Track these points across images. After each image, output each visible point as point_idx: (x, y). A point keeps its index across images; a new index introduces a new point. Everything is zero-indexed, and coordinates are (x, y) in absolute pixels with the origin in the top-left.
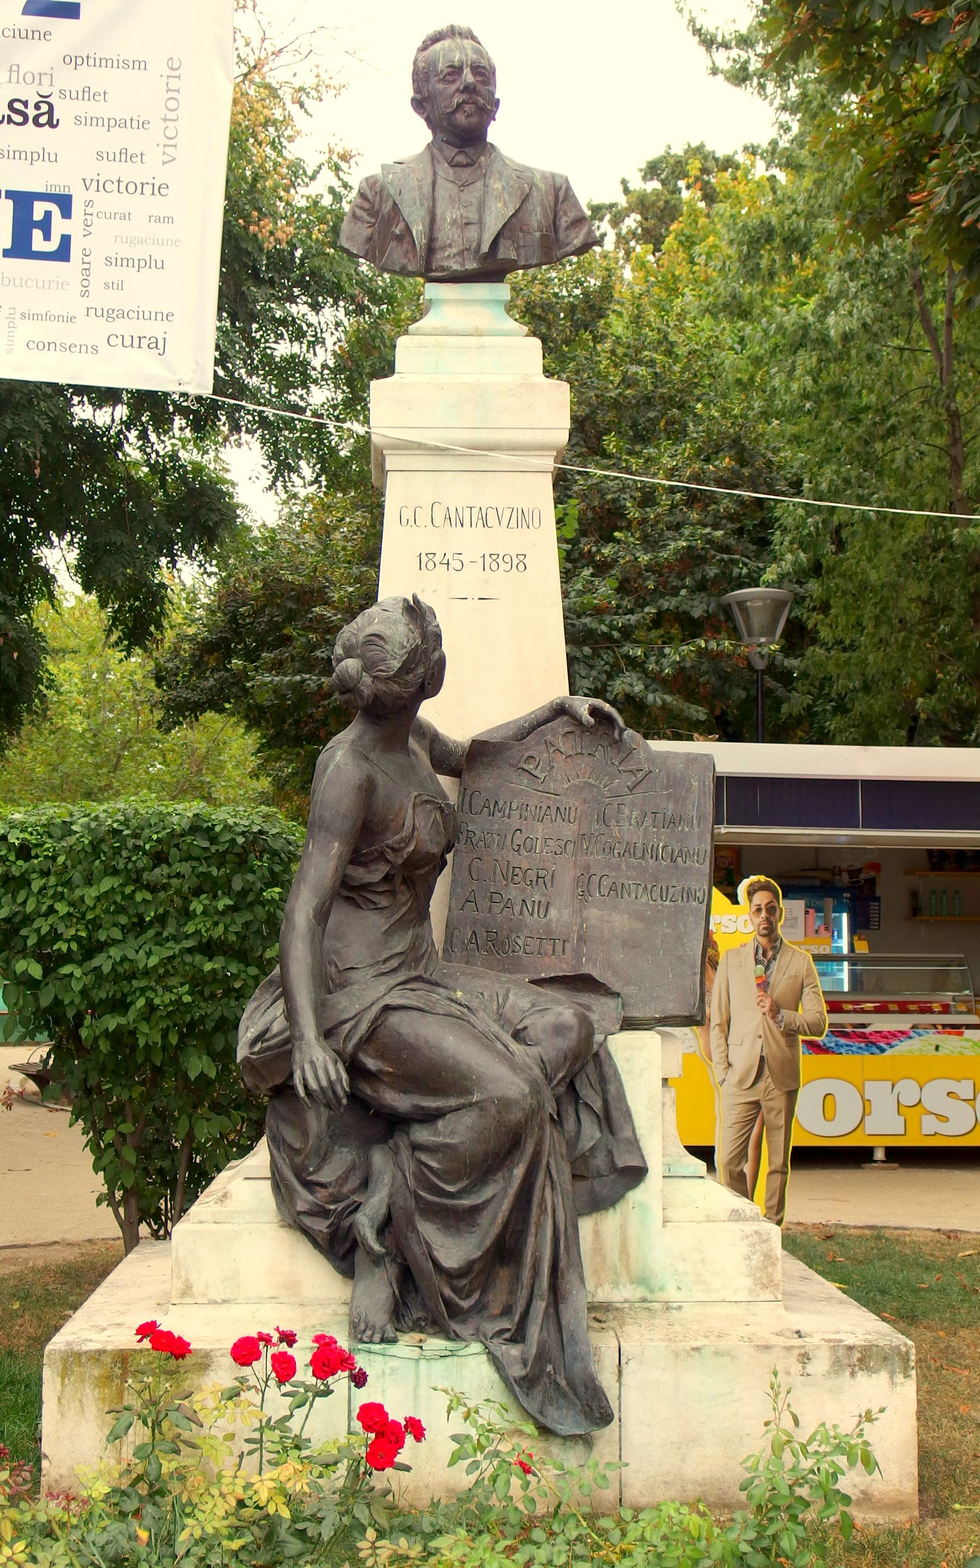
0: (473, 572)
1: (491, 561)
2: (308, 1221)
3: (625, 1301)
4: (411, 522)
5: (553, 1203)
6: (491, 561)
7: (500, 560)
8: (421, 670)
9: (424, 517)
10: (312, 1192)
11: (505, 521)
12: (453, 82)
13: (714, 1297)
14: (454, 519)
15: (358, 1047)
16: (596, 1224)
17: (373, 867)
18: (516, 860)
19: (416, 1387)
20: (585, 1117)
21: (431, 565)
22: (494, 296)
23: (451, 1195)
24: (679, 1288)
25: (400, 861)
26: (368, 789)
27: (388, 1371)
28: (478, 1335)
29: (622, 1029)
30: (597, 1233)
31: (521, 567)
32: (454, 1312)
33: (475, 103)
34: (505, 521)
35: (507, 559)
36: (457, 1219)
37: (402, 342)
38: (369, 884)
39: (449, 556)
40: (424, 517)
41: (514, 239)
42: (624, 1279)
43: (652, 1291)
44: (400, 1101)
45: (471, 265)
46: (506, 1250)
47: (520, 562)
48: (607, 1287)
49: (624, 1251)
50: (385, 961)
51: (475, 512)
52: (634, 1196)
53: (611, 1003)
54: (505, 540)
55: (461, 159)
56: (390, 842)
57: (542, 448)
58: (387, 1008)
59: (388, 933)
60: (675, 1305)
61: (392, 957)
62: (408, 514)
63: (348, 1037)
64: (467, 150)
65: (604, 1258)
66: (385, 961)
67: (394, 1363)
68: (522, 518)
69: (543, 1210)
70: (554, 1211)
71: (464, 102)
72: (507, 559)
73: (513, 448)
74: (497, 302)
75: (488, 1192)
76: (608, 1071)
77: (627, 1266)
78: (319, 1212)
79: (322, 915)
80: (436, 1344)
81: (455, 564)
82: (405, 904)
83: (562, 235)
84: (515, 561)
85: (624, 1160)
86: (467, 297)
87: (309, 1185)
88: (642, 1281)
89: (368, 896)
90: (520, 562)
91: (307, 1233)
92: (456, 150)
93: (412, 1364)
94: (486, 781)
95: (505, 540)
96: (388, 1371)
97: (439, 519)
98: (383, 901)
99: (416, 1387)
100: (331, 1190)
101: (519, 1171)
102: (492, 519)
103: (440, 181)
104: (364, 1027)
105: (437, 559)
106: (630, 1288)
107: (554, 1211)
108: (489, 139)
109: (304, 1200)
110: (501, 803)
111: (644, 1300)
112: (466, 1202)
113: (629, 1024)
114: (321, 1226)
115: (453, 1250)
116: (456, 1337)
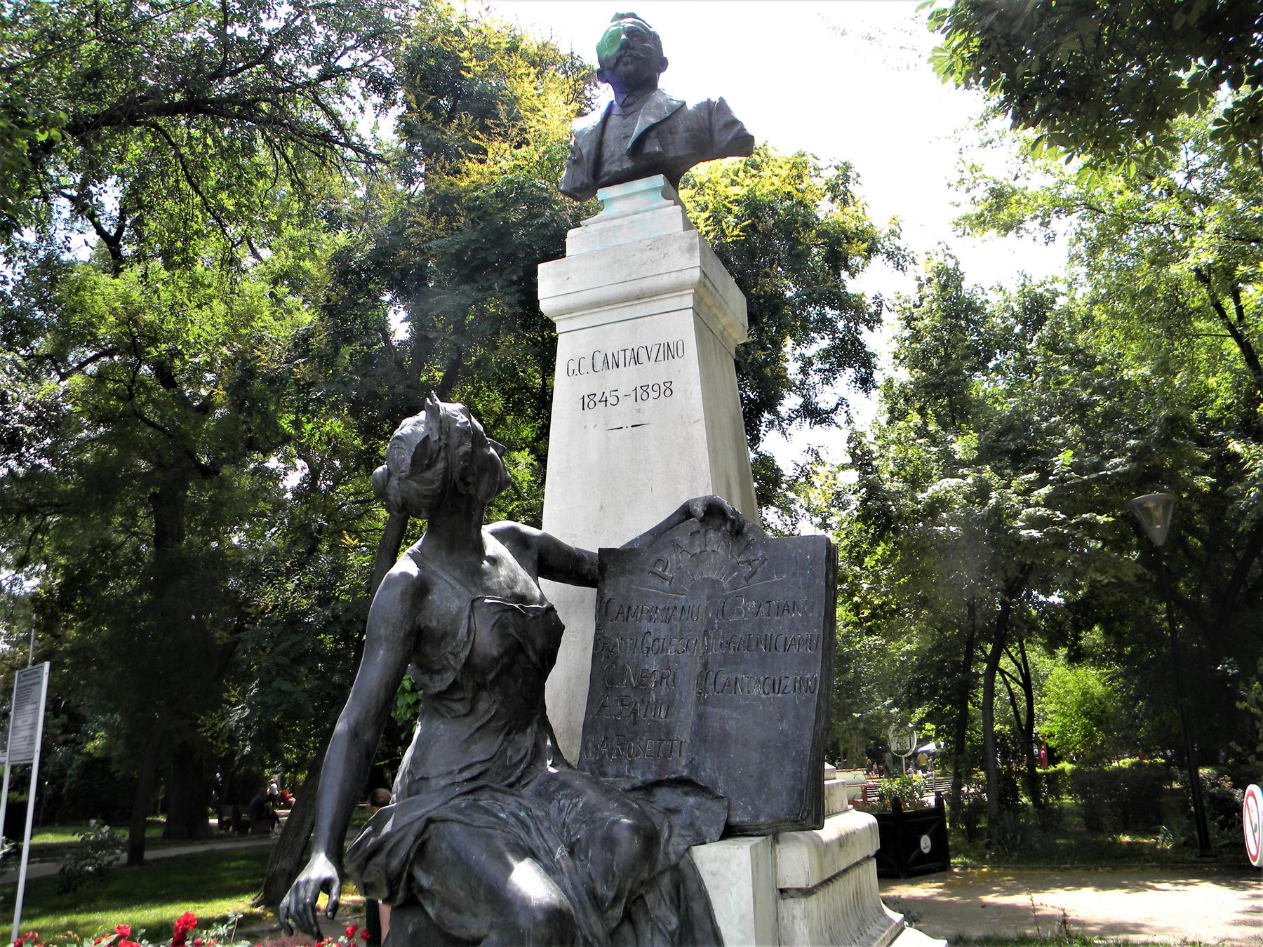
0: (627, 405)
1: (641, 393)
4: (576, 371)
6: (641, 393)
7: (650, 390)
8: (440, 465)
11: (653, 356)
14: (611, 363)
22: (651, 186)
25: (459, 667)
31: (668, 392)
34: (653, 356)
35: (656, 388)
37: (571, 233)
38: (441, 693)
41: (660, 137)
45: (628, 164)
50: (461, 771)
51: (628, 353)
53: (717, 807)
54: (652, 372)
58: (430, 821)
59: (470, 740)
68: (670, 351)
72: (656, 388)
74: (655, 189)
81: (612, 400)
83: (716, 136)
94: (618, 587)
95: (652, 372)
98: (460, 708)
102: (643, 357)
104: (410, 839)
105: (597, 399)
108: (659, 86)
110: (634, 608)
113: (730, 832)
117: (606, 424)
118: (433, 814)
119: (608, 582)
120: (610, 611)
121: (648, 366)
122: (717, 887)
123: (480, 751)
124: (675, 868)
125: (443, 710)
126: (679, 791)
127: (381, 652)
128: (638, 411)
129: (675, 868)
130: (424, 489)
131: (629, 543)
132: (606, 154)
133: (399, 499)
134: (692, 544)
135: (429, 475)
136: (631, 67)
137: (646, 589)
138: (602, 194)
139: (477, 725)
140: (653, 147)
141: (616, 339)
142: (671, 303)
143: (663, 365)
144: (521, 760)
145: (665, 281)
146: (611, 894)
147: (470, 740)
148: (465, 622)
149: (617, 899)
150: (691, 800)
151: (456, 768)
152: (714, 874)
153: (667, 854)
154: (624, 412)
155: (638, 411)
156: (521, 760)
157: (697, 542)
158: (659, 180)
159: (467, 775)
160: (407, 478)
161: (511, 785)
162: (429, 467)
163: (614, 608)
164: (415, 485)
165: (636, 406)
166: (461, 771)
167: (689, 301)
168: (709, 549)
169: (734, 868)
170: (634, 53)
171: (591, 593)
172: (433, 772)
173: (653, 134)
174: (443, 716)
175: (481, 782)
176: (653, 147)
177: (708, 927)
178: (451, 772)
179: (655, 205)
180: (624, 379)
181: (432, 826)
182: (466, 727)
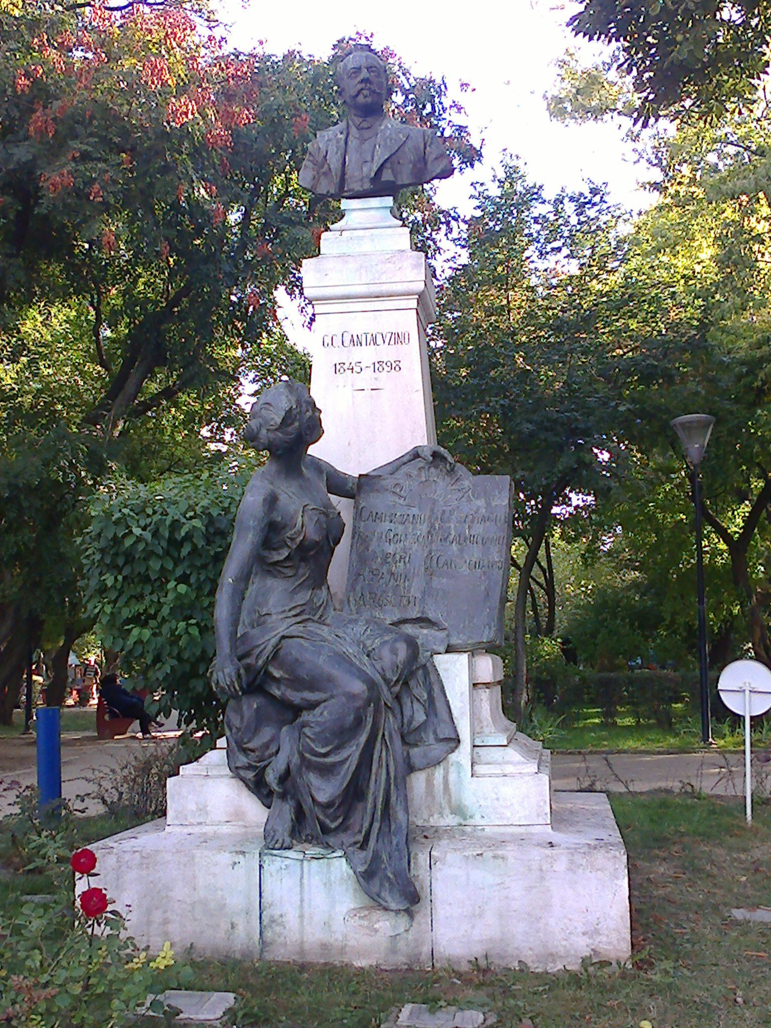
0: (368, 373)
2: (242, 773)
5: (387, 760)
6: (378, 366)
8: (297, 424)
9: (337, 341)
10: (247, 756)
11: (387, 341)
12: (356, 77)
13: (505, 822)
14: (356, 341)
15: (267, 663)
17: (281, 551)
18: (390, 549)
19: (302, 878)
20: (416, 705)
21: (342, 370)
22: (383, 205)
23: (325, 755)
24: (483, 817)
25: (294, 547)
26: (272, 501)
27: (284, 867)
28: (341, 846)
29: (447, 652)
30: (429, 782)
31: (397, 368)
32: (325, 830)
34: (387, 341)
35: (389, 364)
36: (326, 771)
38: (278, 561)
39: (353, 364)
40: (337, 341)
42: (447, 811)
43: (465, 819)
44: (295, 697)
45: (367, 186)
46: (355, 792)
47: (395, 366)
48: (436, 816)
50: (290, 610)
51: (369, 337)
54: (387, 352)
55: (365, 125)
56: (288, 535)
57: (407, 294)
58: (283, 637)
61: (295, 607)
62: (328, 340)
63: (257, 658)
64: (367, 119)
65: (434, 798)
67: (288, 862)
68: (398, 338)
69: (380, 766)
70: (387, 765)
71: (362, 89)
72: (389, 364)
73: (390, 295)
75: (344, 754)
77: (449, 801)
78: (249, 767)
79: (244, 578)
80: (314, 850)
81: (357, 369)
84: (394, 365)
85: (445, 732)
87: (245, 751)
88: (459, 810)
89: (281, 569)
90: (395, 366)
91: (243, 780)
92: (361, 120)
93: (299, 863)
95: (387, 352)
96: (284, 867)
97: (347, 343)
98: (289, 572)
99: (302, 878)
100: (257, 753)
101: (363, 739)
102: (379, 340)
103: (351, 137)
104: (270, 648)
105: (346, 367)
106: (451, 817)
107: (387, 765)
109: (242, 760)
111: (461, 825)
112: (329, 760)
113: (450, 650)
114: (250, 775)
115: (325, 790)
116: (327, 846)
117: (353, 386)
118: (284, 633)
119: (362, 495)
120: (363, 514)
124: (424, 667)
125: (275, 573)
126: (417, 626)
127: (251, 536)
128: (376, 379)
129: (424, 667)
130: (287, 438)
132: (349, 172)
133: (267, 442)
134: (419, 476)
135: (290, 429)
136: (369, 100)
138: (345, 204)
139: (297, 584)
140: (387, 176)
141: (360, 324)
142: (403, 304)
143: (393, 348)
144: (321, 606)
145: (399, 288)
146: (395, 679)
147: (294, 592)
148: (300, 519)
149: (397, 681)
150: (425, 631)
151: (287, 608)
152: (446, 670)
154: (366, 378)
155: (376, 379)
156: (321, 606)
157: (423, 474)
158: (389, 201)
159: (293, 613)
160: (276, 430)
163: (365, 514)
164: (280, 435)
165: (375, 375)
166: (290, 610)
167: (414, 304)
168: (431, 479)
169: (458, 666)
170: (373, 87)
172: (273, 611)
173: (388, 165)
174: (275, 577)
176: (387, 176)
177: (129, 826)
178: (284, 611)
179: (387, 224)
180: (366, 355)
181: (283, 641)
182: (290, 585)
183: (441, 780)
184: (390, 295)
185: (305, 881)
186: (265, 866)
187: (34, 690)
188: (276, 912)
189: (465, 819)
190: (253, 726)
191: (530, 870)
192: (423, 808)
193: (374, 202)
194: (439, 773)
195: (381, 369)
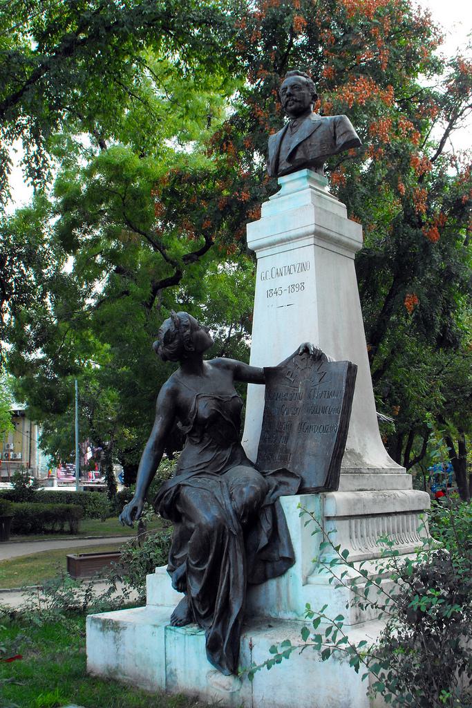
3: (289, 619)
9: (269, 274)
14: (279, 274)
16: (278, 583)
19: (185, 647)
22: (302, 176)
30: (278, 587)
33: (293, 100)
43: (299, 616)
45: (288, 165)
48: (282, 612)
49: (288, 598)
50: (197, 466)
52: (292, 570)
54: (295, 278)
57: (307, 235)
60: (308, 623)
61: (200, 464)
62: (264, 275)
66: (197, 466)
67: (178, 635)
68: (303, 267)
70: (227, 554)
73: (289, 240)
74: (304, 177)
76: (278, 513)
81: (279, 292)
82: (208, 441)
86: (293, 179)
88: (295, 611)
90: (302, 286)
95: (295, 278)
102: (292, 270)
111: (296, 620)
121: (295, 275)
122: (288, 513)
123: (209, 456)
131: (366, 330)
137: (282, 387)
138: (281, 180)
153: (270, 499)
154: (284, 298)
159: (199, 468)
161: (218, 473)
162: (172, 342)
171: (263, 386)
173: (300, 148)
175: (203, 470)
176: (299, 156)
177: (284, 526)
180: (285, 281)
182: (197, 450)
183: (275, 588)
184: (289, 240)
185: (186, 649)
186: (167, 636)
187: (464, 473)
188: (173, 668)
189: (299, 616)
190: (179, 544)
191: (307, 658)
192: (275, 606)
193: (297, 175)
194: (283, 580)
195: (293, 291)
